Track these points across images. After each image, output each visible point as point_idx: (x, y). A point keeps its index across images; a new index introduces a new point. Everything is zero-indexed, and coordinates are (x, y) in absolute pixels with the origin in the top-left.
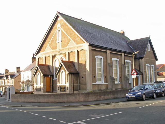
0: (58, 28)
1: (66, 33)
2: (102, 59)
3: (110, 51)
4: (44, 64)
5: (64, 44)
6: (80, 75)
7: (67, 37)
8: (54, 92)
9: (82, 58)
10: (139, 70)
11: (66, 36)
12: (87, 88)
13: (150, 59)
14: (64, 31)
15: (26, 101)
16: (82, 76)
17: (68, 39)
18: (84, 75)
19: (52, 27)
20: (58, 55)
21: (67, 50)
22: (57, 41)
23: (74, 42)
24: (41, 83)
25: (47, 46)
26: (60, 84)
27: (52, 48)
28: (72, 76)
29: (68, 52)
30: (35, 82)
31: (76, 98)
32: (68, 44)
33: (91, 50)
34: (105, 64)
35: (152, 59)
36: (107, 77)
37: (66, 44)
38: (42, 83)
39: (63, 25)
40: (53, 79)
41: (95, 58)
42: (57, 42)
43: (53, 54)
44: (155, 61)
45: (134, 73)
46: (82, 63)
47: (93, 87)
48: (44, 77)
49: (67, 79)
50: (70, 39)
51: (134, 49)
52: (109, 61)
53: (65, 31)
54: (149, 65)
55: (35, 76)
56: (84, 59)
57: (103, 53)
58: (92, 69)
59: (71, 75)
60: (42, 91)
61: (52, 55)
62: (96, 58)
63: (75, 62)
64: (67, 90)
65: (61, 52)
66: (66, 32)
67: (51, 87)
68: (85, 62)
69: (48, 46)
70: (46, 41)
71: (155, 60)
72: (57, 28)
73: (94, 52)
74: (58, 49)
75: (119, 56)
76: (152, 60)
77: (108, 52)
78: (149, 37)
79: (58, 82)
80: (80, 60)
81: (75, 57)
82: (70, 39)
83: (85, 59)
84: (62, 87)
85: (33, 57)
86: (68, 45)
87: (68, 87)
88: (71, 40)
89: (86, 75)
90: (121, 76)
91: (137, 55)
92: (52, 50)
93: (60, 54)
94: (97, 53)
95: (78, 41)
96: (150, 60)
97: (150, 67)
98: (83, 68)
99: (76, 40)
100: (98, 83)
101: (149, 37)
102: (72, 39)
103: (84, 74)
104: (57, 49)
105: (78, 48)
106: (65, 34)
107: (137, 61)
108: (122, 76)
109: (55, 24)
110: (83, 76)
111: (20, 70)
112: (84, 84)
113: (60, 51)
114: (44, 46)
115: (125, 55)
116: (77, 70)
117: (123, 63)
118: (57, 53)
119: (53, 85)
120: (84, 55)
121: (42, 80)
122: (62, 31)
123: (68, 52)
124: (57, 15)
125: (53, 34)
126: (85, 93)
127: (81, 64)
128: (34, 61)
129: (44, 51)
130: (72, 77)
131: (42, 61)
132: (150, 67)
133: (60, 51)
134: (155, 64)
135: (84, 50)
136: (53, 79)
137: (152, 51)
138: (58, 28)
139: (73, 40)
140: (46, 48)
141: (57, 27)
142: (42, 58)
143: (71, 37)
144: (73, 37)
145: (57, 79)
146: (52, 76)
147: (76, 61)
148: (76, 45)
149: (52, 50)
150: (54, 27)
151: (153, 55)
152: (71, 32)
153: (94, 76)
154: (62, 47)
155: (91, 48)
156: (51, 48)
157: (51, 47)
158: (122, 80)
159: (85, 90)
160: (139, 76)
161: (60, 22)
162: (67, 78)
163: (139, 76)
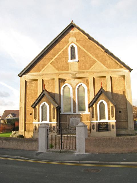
5: (83, 65)
7: (90, 57)
11: (87, 55)
12: (129, 126)
16: (119, 110)
17: (92, 59)
19: (58, 40)
22: (68, 59)
25: (46, 65)
26: (97, 120)
29: (42, 79)
37: (87, 65)
38: (54, 118)
40: (60, 114)
43: (62, 77)
46: (117, 93)
49: (112, 114)
55: (35, 107)
56: (122, 88)
63: (54, 94)
65: (78, 76)
66: (87, 50)
68: (124, 92)
70: (45, 57)
74: (70, 71)
80: (114, 89)
84: (101, 125)
87: (113, 126)
92: (57, 72)
93: (76, 78)
99: (106, 62)
105: (112, 73)
106: (85, 52)
109: (65, 36)
110: (121, 111)
112: (122, 121)
113: (76, 74)
114: (40, 63)
118: (70, 76)
120: (121, 83)
121: (54, 114)
123: (42, 79)
125: (60, 49)
127: (117, 94)
129: (39, 70)
133: (76, 74)
136: (60, 114)
138: (70, 42)
140: (43, 67)
141: (68, 41)
147: (110, 91)
150: (63, 40)
152: (97, 51)
159: (124, 128)
162: (112, 112)
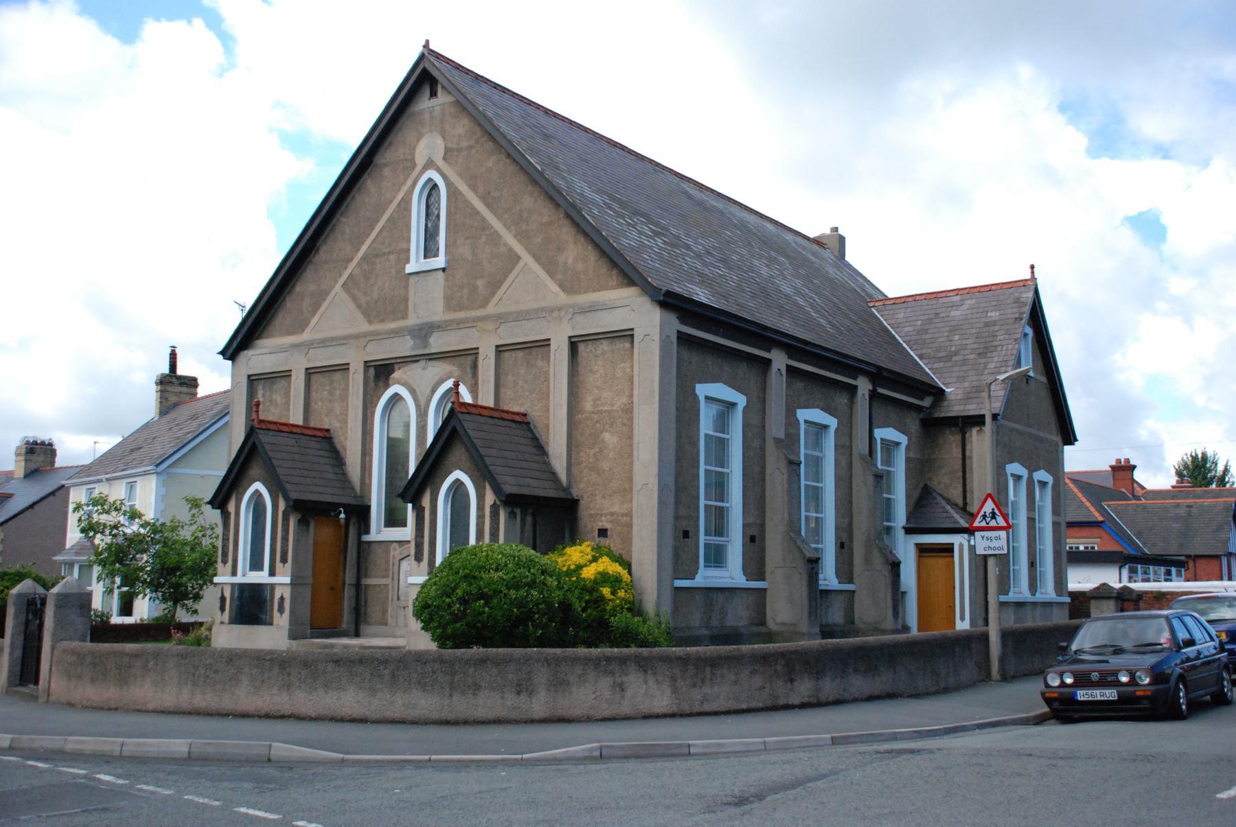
0: (425, 168)
1: (488, 206)
2: (740, 408)
3: (790, 357)
4: (301, 423)
6: (584, 513)
7: (495, 238)
8: (364, 628)
9: (606, 395)
10: (960, 502)
11: (485, 226)
13: (1034, 431)
14: (473, 187)
15: (202, 700)
18: (612, 514)
20: (414, 359)
21: (490, 326)
23: (543, 275)
24: (279, 565)
27: (369, 312)
28: (529, 519)
30: (225, 554)
31: (622, 687)
32: (494, 286)
33: (674, 339)
34: (756, 444)
35: (1041, 434)
36: (763, 540)
38: (284, 560)
39: (464, 144)
41: (699, 402)
42: (410, 268)
43: (380, 352)
44: (1057, 445)
45: (993, 523)
47: (676, 609)
48: (303, 522)
50: (518, 248)
51: (921, 357)
52: (776, 428)
53: (481, 189)
54: (1023, 472)
56: (621, 401)
57: (742, 369)
58: (677, 478)
59: (518, 512)
60: (282, 621)
61: (249, 376)
62: (702, 399)
64: (276, 614)
65: (437, 343)
67: (348, 592)
69: (338, 287)
71: (1058, 439)
72: (414, 165)
73: (695, 358)
75: (842, 400)
76: (1041, 440)
77: (779, 360)
78: (1028, 276)
79: (225, 562)
81: (547, 380)
82: (518, 248)
83: (624, 400)
85: (166, 371)
86: (493, 294)
88: (527, 258)
89: (629, 514)
90: (845, 536)
91: (952, 397)
92: (365, 327)
94: (710, 362)
95: (580, 266)
96: (1030, 435)
97: (1030, 481)
98: (605, 465)
99: (561, 258)
100: (706, 577)
101: (1028, 276)
102: (529, 250)
103: (616, 509)
104: (405, 317)
106: (478, 213)
107: (952, 438)
108: (851, 537)
111: (53, 463)
114: (305, 286)
115: (874, 395)
116: (563, 477)
117: (861, 446)
118: (405, 347)
119: (358, 586)
122: (453, 192)
124: (421, 67)
125: (380, 209)
126: (765, 659)
128: (173, 399)
130: (529, 526)
131: (278, 398)
132: (1030, 481)
134: (1055, 465)
135: (627, 335)
136: (365, 538)
137: (1044, 379)
138: (420, 161)
139: (537, 258)
140: (316, 307)
141: (413, 160)
142: (283, 382)
143: (522, 237)
144: (538, 239)
145: (406, 533)
146: (361, 513)
148: (563, 298)
149: (370, 322)
151: (1047, 406)
153: (684, 525)
154: (451, 303)
155: (672, 318)
156: (359, 306)
157: (363, 300)
158: (851, 564)
160: (961, 546)
161: (442, 121)
163: (961, 546)
